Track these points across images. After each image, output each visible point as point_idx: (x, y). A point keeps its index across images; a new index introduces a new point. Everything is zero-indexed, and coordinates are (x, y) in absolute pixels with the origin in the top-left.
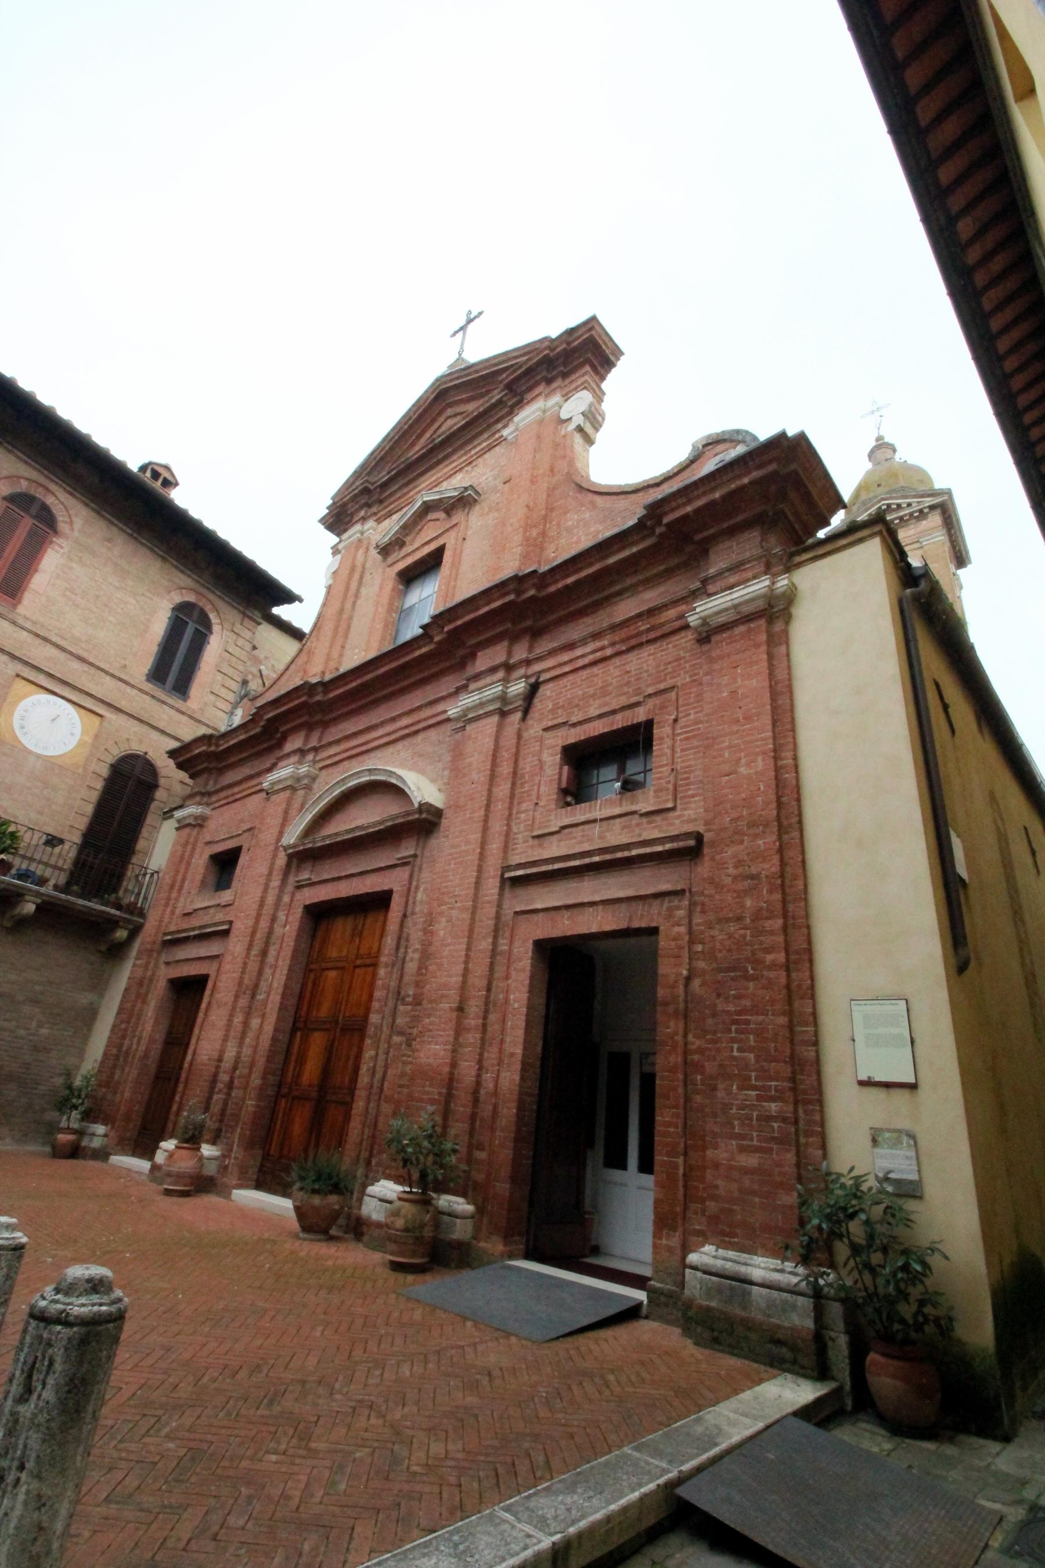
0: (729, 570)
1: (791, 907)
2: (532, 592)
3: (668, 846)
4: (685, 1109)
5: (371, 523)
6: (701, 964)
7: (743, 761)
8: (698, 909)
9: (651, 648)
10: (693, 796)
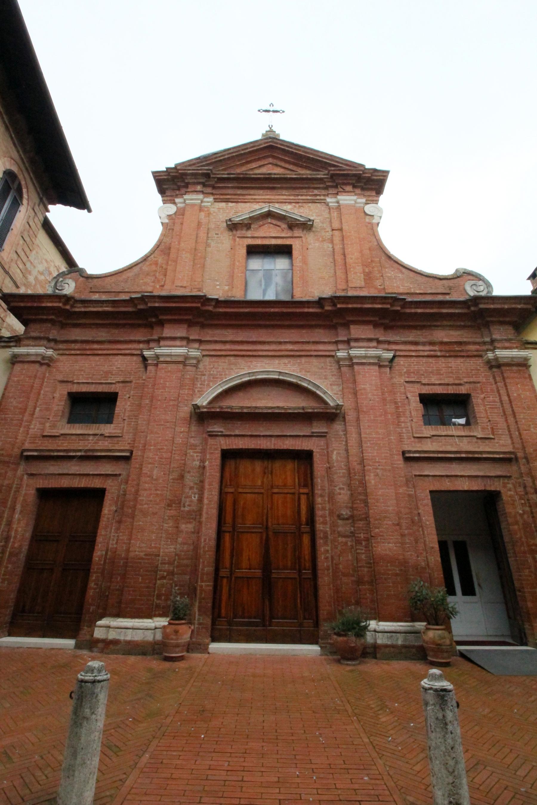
0: (506, 340)
2: (399, 308)
3: (501, 456)
5: (211, 199)
7: (532, 426)
9: (462, 360)
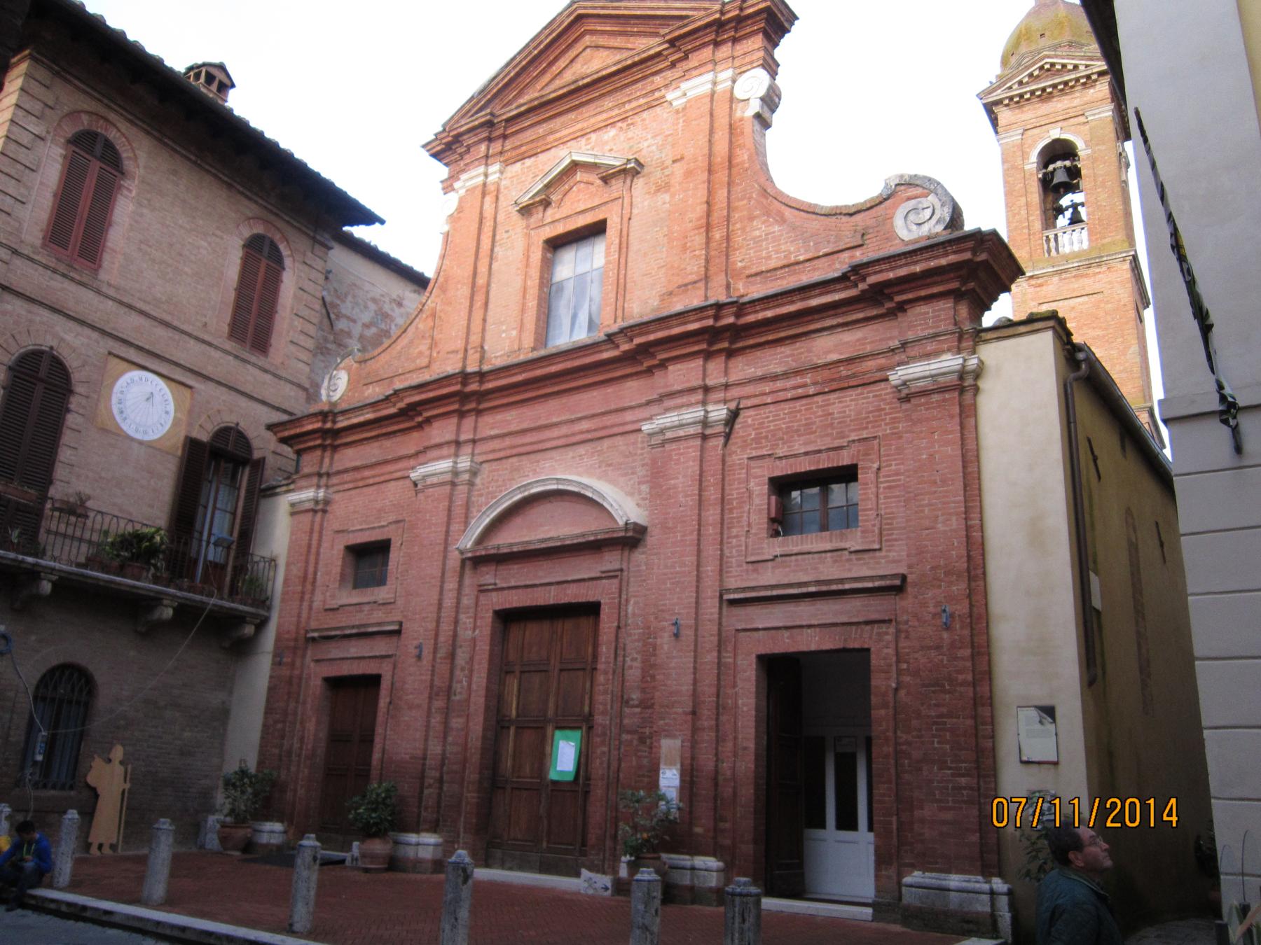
1: (976, 639)
2: (731, 320)
3: (877, 584)
4: (897, 784)
6: (907, 679)
7: (941, 519)
8: (903, 635)
10: (896, 540)
